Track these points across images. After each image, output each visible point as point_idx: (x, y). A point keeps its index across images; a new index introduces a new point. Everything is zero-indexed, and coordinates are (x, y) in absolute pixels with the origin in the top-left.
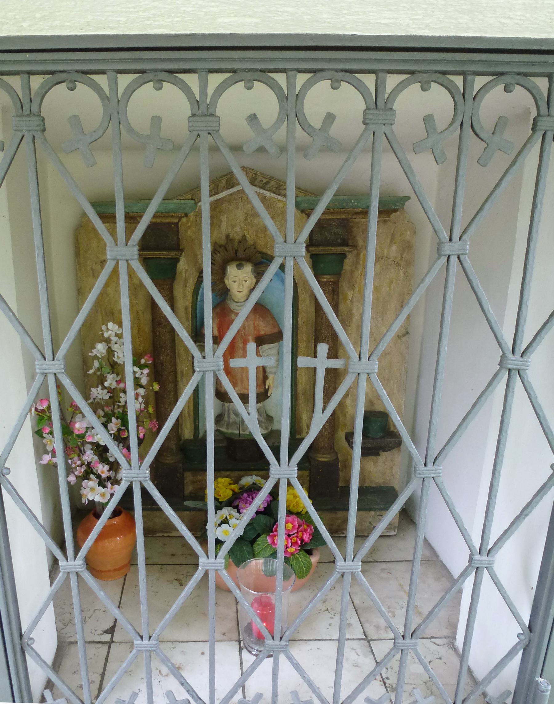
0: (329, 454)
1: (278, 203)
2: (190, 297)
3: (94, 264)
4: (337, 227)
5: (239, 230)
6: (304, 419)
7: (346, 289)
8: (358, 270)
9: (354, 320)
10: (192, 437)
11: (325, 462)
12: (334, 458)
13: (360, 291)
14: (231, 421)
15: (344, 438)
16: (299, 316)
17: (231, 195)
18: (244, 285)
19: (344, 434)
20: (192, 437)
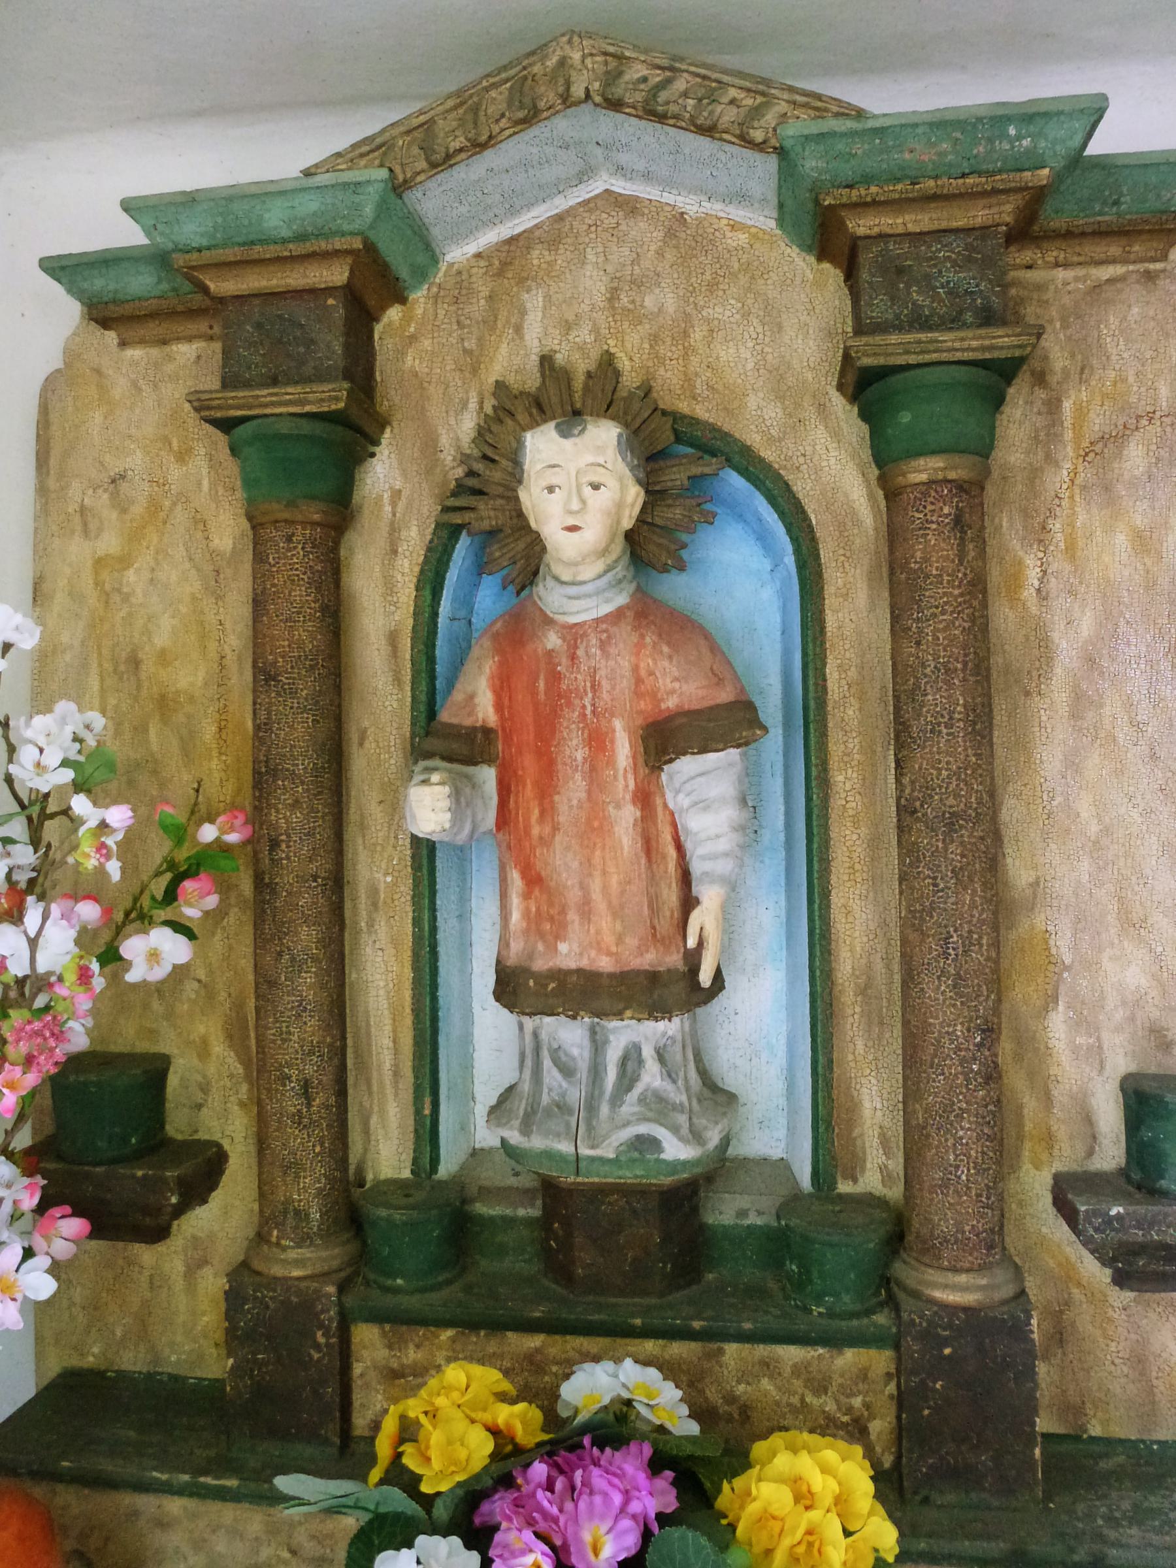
0: (980, 1269)
1: (729, 234)
2: (407, 592)
3: (90, 492)
4: (955, 264)
5: (589, 339)
6: (867, 1104)
7: (1015, 544)
8: (1057, 465)
9: (1058, 671)
10: (406, 1174)
11: (966, 1309)
12: (1008, 1291)
13: (1071, 550)
14: (545, 1099)
15: (1048, 1199)
16: (830, 660)
17: (559, 218)
18: (590, 502)
19: (1049, 1181)
20: (406, 1174)
